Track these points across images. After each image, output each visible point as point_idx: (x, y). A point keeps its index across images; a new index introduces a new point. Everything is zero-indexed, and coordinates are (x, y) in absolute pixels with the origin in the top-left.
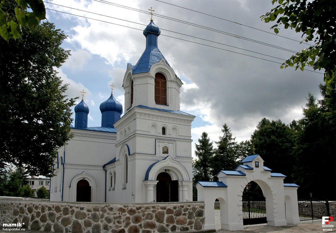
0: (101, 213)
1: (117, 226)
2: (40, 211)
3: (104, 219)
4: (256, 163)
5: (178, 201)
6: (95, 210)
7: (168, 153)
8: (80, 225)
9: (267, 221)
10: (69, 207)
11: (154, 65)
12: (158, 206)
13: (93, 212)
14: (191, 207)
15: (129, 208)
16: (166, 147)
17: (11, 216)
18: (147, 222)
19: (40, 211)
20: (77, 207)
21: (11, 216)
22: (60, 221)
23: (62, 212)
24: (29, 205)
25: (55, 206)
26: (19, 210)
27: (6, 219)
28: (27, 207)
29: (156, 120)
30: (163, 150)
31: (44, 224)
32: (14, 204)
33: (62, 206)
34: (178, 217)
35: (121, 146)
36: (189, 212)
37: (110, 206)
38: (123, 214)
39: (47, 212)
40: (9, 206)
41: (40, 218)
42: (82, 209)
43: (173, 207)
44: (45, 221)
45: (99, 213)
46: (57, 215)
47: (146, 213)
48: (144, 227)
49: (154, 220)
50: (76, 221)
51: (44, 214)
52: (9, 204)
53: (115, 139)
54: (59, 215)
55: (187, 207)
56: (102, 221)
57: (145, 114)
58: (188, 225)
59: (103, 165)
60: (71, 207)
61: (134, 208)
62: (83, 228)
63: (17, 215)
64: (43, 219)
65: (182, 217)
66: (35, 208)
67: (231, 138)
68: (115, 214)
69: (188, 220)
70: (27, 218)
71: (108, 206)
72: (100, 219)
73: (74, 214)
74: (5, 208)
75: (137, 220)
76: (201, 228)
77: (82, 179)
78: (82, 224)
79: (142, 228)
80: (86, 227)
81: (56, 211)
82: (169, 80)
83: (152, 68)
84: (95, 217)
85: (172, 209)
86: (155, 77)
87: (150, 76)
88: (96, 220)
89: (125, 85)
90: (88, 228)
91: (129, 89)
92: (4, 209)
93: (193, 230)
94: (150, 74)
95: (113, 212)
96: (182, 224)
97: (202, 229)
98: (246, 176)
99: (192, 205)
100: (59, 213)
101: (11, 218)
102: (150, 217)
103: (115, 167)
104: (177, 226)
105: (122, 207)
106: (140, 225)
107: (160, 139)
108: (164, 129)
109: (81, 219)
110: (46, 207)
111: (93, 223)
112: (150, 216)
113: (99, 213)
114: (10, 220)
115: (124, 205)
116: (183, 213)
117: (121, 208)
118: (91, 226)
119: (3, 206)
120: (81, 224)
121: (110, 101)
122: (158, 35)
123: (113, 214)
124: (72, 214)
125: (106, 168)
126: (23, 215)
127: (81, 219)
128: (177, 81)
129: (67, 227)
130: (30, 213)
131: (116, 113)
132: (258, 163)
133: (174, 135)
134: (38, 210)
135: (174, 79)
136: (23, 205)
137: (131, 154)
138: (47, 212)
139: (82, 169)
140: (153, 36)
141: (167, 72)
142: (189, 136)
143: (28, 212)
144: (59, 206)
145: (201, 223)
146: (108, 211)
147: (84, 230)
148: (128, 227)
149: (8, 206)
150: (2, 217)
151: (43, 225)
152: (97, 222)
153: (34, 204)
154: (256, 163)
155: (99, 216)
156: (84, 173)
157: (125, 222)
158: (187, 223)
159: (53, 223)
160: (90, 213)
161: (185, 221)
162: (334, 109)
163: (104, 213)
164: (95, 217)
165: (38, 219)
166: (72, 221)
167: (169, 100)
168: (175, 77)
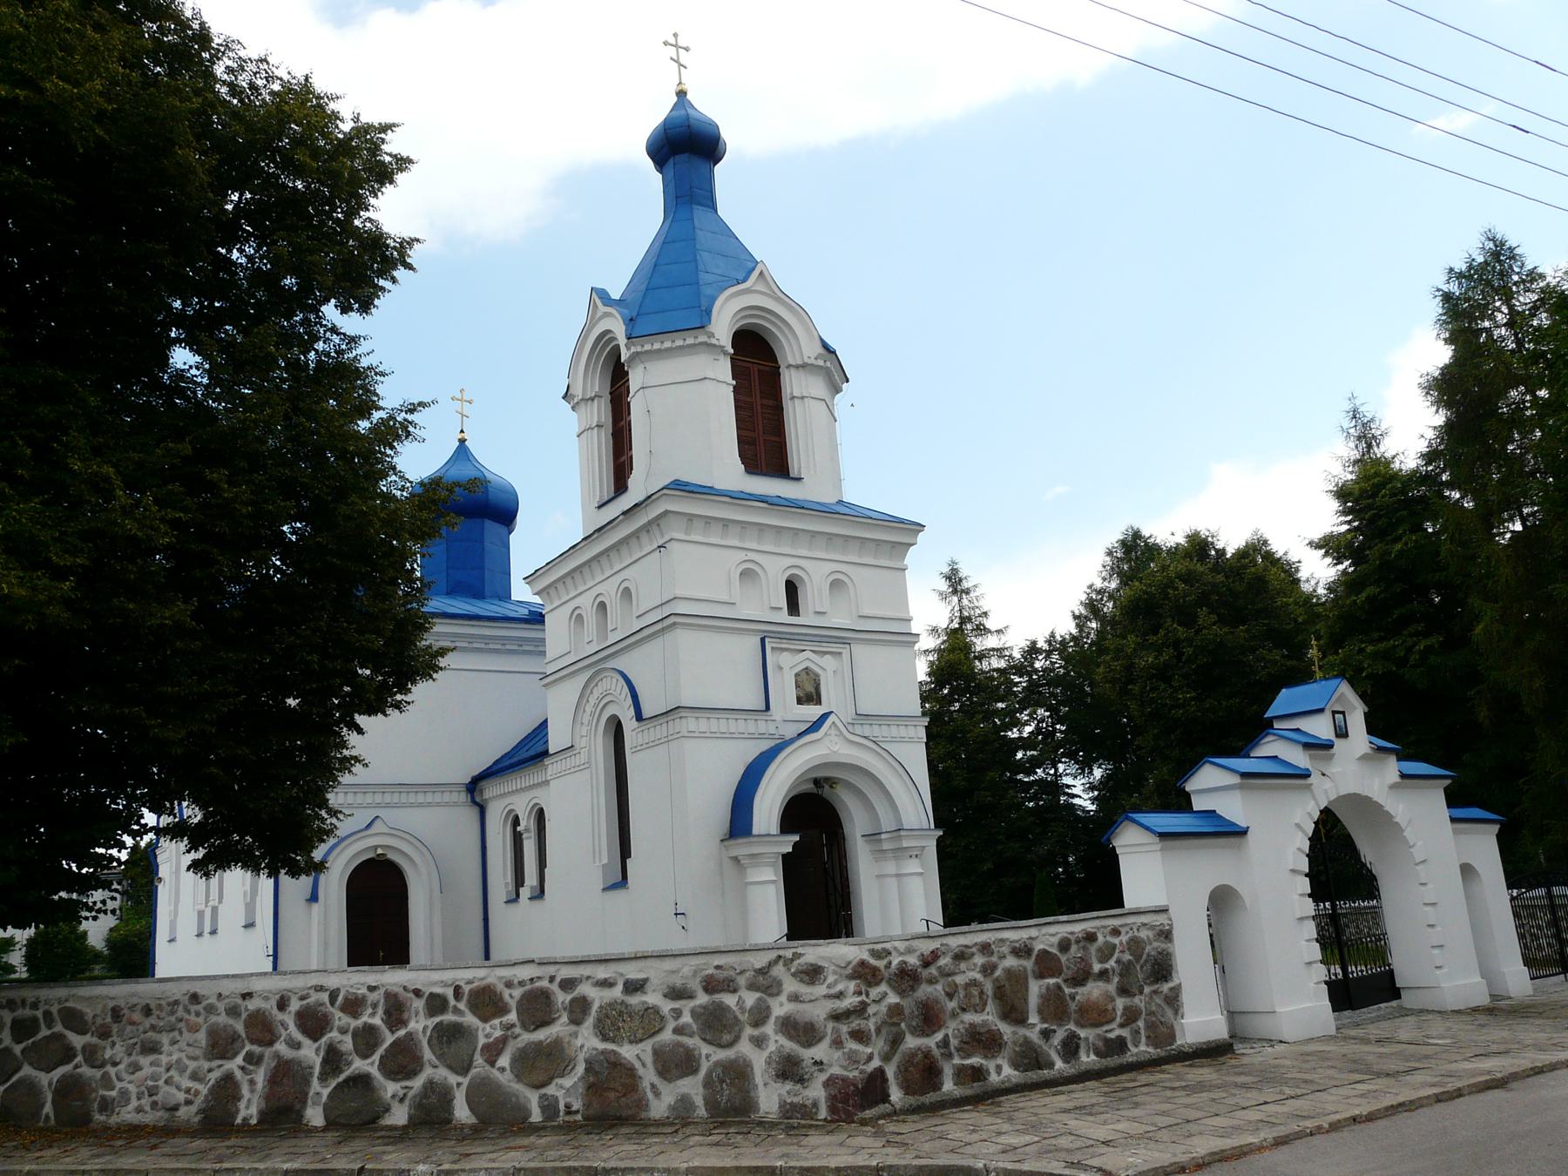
0: (750, 998)
1: (852, 1059)
2: (377, 1021)
3: (769, 1028)
4: (1336, 715)
6: (711, 986)
7: (819, 702)
8: (630, 1071)
10: (555, 987)
12: (1002, 940)
13: (702, 999)
14: (1124, 938)
15: (896, 961)
16: (808, 674)
17: (192, 1065)
18: (970, 1024)
19: (377, 1021)
20: (606, 980)
21: (192, 1065)
22: (504, 1061)
23: (512, 1017)
24: (302, 998)
25: (466, 989)
26: (240, 1027)
27: (161, 1083)
28: (295, 1005)
29: (754, 546)
30: (797, 686)
31: (406, 1087)
32: (213, 1000)
33: (509, 985)
34: (1080, 990)
36: (1118, 962)
37: (802, 960)
38: (875, 992)
39: (419, 1024)
40: (180, 1012)
41: (376, 1057)
42: (634, 987)
43: (1055, 940)
44: (411, 1074)
45: (740, 997)
46: (487, 1032)
47: (960, 980)
48: (958, 1051)
49: (989, 1016)
50: (603, 1052)
51: (402, 1033)
52: (176, 1003)
53: (537, 649)
54: (498, 1033)
55: (1110, 939)
56: (759, 1042)
57: (708, 520)
58: (1122, 1026)
59: (468, 780)
60: (568, 985)
61: (913, 960)
62: (649, 1086)
63: (228, 1059)
64: (402, 1062)
65: (1093, 991)
66: (343, 1009)
67: (438, 666)
68: (840, 995)
69: (1120, 1003)
70: (299, 1063)
71: (792, 960)
72: (749, 1031)
73: (590, 1021)
74: (153, 1027)
75: (929, 1018)
76: (1172, 1037)
77: (371, 855)
78: (644, 1065)
79: (950, 1056)
80: (665, 1079)
81: (475, 1014)
83: (719, 314)
84: (716, 1024)
85: (1054, 951)
86: (732, 351)
87: (714, 345)
88: (727, 1037)
89: (578, 391)
90: (680, 1082)
91: (600, 411)
92: (145, 1032)
93: (1143, 1048)
94: (712, 335)
95: (829, 987)
96: (1102, 1024)
97: (1179, 1042)
98: (1310, 780)
99: (1127, 925)
100: (496, 1022)
101: (195, 1077)
102: (977, 1000)
103: (547, 783)
104: (1082, 1033)
105: (866, 956)
106: (945, 1043)
107: (781, 637)
108: (792, 588)
109: (635, 1041)
110: (411, 995)
111: (708, 1056)
112: (975, 992)
113: (740, 997)
114: (190, 1084)
115: (871, 946)
116: (1097, 967)
117: (863, 963)
118: (694, 1071)
119: (137, 1016)
120: (637, 1065)
122: (717, 160)
123: (828, 997)
124: (576, 1021)
125: (481, 792)
126: (268, 1052)
127: (631, 1042)
128: (828, 364)
129: (550, 1090)
130: (315, 1040)
131: (491, 527)
132: (1341, 716)
133: (840, 618)
134: (365, 1019)
135: (816, 359)
136: (266, 999)
138: (419, 1024)
139: (369, 806)
142: (902, 615)
143: (298, 1035)
144: (494, 985)
145: (1169, 1012)
146: (790, 985)
147: (657, 1094)
148: (897, 1058)
149: (172, 1013)
150: (133, 1073)
151: (401, 1093)
152: (730, 1045)
153: (338, 989)
154: (1336, 715)
155: (744, 1018)
156: (378, 823)
157: (884, 1031)
158: (1118, 1019)
159: (460, 1079)
160: (686, 1006)
161: (1110, 1007)
163: (771, 995)
164: (716, 1024)
165: (369, 1066)
166: (581, 1057)
168: (820, 350)
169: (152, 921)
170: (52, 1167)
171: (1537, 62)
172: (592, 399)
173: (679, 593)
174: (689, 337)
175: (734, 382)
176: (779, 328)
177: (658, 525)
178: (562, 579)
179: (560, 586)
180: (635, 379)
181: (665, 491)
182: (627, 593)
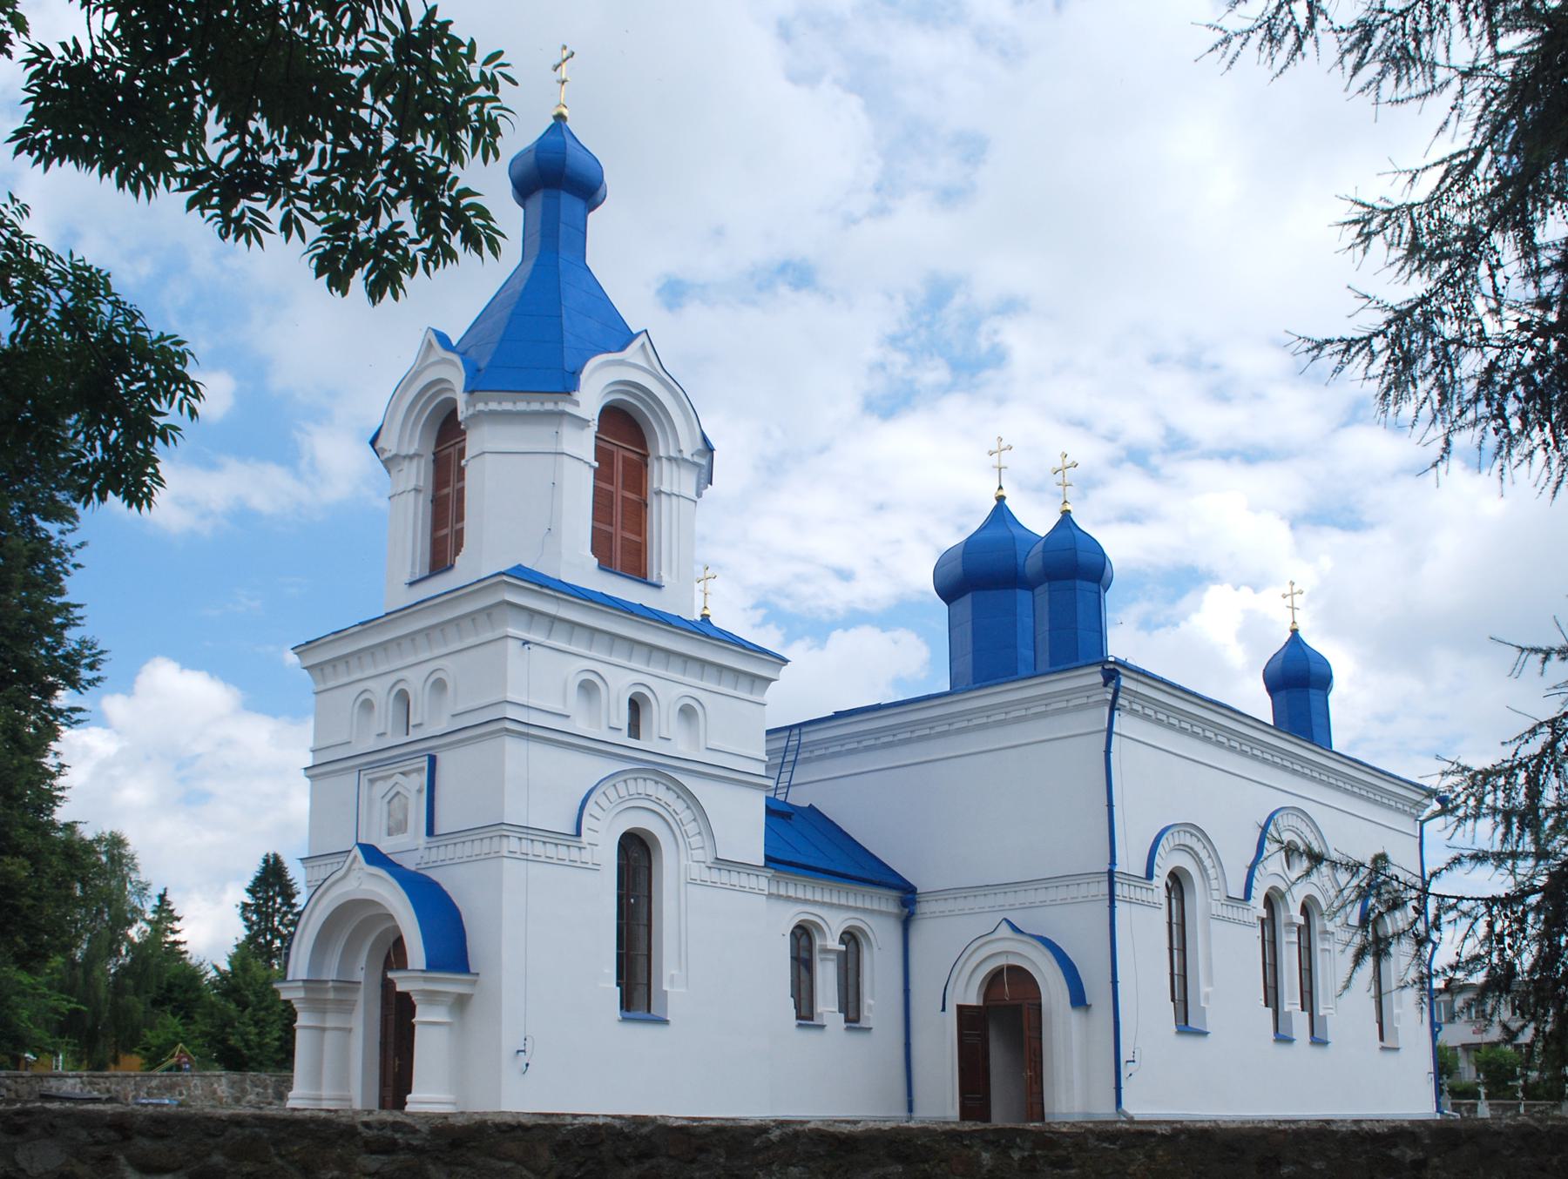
81: (954, 1130)
89: (389, 443)
94: (577, 404)
121: (997, 532)
137: (437, 832)
140: (568, 202)
168: (699, 445)
169: (1043, 665)
170: (138, 1073)
172: (411, 457)
173: (511, 697)
174: (535, 401)
175: (596, 464)
177: (347, 662)
180: (476, 441)
181: (505, 578)
182: (439, 686)
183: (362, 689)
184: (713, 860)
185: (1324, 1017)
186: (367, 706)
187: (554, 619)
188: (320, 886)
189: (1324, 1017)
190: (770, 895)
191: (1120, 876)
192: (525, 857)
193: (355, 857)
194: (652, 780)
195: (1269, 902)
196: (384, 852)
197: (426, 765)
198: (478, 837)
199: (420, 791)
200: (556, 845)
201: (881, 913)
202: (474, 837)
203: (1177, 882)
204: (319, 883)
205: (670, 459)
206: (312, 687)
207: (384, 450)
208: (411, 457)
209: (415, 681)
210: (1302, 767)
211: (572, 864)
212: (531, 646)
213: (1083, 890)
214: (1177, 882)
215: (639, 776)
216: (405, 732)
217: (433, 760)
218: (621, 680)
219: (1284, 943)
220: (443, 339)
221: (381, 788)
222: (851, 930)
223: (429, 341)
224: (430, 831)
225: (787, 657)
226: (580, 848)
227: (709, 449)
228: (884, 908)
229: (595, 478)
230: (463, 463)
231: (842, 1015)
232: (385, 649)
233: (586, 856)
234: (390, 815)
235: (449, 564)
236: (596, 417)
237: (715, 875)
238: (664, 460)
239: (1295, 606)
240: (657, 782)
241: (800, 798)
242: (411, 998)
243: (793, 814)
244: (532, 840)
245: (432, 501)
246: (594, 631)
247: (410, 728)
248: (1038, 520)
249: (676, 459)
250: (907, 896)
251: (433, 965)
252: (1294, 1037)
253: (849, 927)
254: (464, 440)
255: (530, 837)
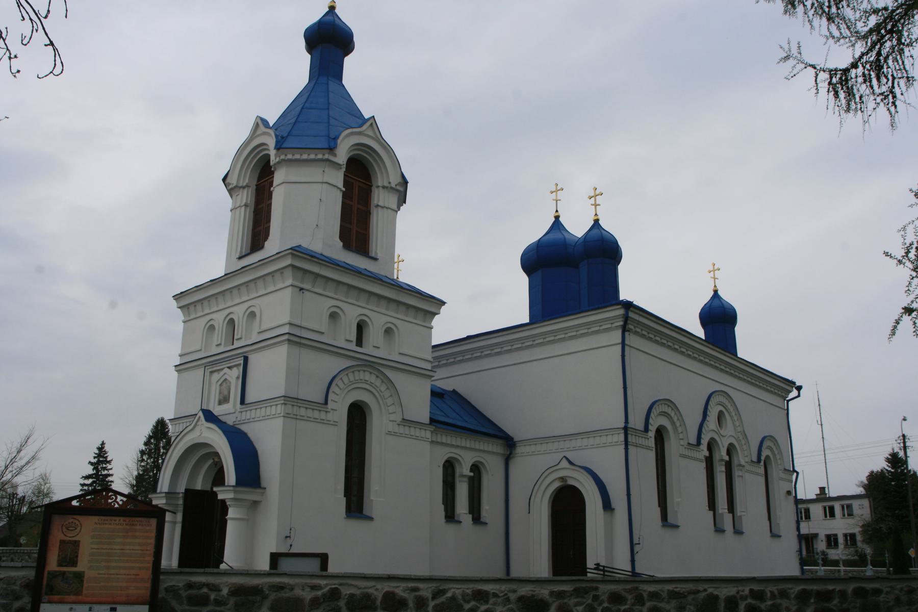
5: (76, 566)
9: (470, 513)
11: (350, 131)
35: (349, 363)
82: (380, 184)
89: (233, 180)
108: (361, 328)
141: (374, 154)
162: (802, 1)
167: (377, 245)
168: (399, 180)
171: (10, 67)
172: (244, 187)
175: (344, 189)
176: (377, 164)
177: (202, 303)
178: (238, 287)
179: (278, 275)
183: (208, 320)
184: (401, 420)
185: (741, 516)
186: (212, 328)
187: (318, 276)
188: (178, 436)
189: (741, 516)
190: (432, 442)
191: (630, 430)
192: (295, 417)
193: (200, 417)
194: (368, 371)
195: (710, 447)
196: (216, 414)
197: (242, 362)
198: (305, 406)
199: (238, 378)
200: (313, 409)
201: (493, 453)
202: (271, 404)
203: (660, 435)
204: (178, 434)
205: (384, 187)
206: (182, 318)
207: (229, 184)
208: (244, 187)
209: (239, 313)
210: (720, 365)
211: (322, 422)
212: (304, 291)
213: (610, 439)
214: (660, 435)
215: (362, 369)
216: (232, 343)
217: (246, 359)
218: (352, 313)
219: (736, 477)
220: (265, 122)
221: (216, 376)
222: (476, 463)
223: (257, 123)
224: (243, 402)
225: (445, 301)
226: (326, 412)
227: (405, 182)
228: (499, 451)
229: (343, 197)
230: (272, 189)
231: (471, 516)
232: (224, 295)
233: (330, 416)
234: (220, 393)
235: (261, 246)
236: (345, 163)
237: (402, 430)
238: (381, 188)
239: (716, 277)
240: (371, 373)
241: (448, 385)
242: (226, 503)
243: (444, 394)
244: (300, 407)
245: (254, 212)
246: (339, 283)
247: (235, 341)
248: (577, 227)
249: (387, 187)
250: (509, 443)
251: (240, 482)
252: (725, 529)
253: (475, 462)
254: (273, 177)
255: (298, 404)
